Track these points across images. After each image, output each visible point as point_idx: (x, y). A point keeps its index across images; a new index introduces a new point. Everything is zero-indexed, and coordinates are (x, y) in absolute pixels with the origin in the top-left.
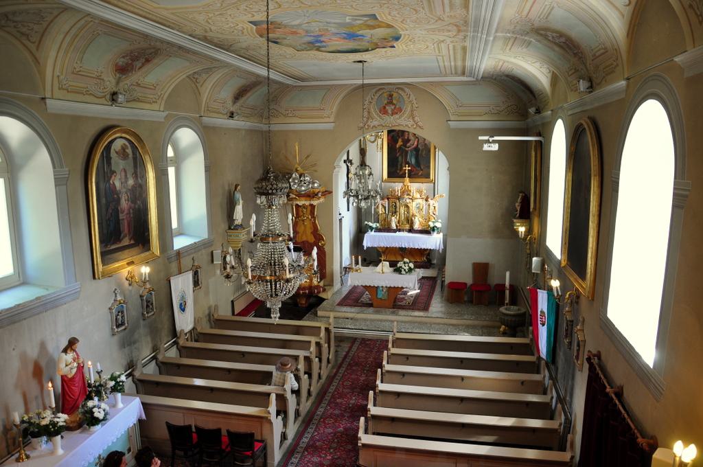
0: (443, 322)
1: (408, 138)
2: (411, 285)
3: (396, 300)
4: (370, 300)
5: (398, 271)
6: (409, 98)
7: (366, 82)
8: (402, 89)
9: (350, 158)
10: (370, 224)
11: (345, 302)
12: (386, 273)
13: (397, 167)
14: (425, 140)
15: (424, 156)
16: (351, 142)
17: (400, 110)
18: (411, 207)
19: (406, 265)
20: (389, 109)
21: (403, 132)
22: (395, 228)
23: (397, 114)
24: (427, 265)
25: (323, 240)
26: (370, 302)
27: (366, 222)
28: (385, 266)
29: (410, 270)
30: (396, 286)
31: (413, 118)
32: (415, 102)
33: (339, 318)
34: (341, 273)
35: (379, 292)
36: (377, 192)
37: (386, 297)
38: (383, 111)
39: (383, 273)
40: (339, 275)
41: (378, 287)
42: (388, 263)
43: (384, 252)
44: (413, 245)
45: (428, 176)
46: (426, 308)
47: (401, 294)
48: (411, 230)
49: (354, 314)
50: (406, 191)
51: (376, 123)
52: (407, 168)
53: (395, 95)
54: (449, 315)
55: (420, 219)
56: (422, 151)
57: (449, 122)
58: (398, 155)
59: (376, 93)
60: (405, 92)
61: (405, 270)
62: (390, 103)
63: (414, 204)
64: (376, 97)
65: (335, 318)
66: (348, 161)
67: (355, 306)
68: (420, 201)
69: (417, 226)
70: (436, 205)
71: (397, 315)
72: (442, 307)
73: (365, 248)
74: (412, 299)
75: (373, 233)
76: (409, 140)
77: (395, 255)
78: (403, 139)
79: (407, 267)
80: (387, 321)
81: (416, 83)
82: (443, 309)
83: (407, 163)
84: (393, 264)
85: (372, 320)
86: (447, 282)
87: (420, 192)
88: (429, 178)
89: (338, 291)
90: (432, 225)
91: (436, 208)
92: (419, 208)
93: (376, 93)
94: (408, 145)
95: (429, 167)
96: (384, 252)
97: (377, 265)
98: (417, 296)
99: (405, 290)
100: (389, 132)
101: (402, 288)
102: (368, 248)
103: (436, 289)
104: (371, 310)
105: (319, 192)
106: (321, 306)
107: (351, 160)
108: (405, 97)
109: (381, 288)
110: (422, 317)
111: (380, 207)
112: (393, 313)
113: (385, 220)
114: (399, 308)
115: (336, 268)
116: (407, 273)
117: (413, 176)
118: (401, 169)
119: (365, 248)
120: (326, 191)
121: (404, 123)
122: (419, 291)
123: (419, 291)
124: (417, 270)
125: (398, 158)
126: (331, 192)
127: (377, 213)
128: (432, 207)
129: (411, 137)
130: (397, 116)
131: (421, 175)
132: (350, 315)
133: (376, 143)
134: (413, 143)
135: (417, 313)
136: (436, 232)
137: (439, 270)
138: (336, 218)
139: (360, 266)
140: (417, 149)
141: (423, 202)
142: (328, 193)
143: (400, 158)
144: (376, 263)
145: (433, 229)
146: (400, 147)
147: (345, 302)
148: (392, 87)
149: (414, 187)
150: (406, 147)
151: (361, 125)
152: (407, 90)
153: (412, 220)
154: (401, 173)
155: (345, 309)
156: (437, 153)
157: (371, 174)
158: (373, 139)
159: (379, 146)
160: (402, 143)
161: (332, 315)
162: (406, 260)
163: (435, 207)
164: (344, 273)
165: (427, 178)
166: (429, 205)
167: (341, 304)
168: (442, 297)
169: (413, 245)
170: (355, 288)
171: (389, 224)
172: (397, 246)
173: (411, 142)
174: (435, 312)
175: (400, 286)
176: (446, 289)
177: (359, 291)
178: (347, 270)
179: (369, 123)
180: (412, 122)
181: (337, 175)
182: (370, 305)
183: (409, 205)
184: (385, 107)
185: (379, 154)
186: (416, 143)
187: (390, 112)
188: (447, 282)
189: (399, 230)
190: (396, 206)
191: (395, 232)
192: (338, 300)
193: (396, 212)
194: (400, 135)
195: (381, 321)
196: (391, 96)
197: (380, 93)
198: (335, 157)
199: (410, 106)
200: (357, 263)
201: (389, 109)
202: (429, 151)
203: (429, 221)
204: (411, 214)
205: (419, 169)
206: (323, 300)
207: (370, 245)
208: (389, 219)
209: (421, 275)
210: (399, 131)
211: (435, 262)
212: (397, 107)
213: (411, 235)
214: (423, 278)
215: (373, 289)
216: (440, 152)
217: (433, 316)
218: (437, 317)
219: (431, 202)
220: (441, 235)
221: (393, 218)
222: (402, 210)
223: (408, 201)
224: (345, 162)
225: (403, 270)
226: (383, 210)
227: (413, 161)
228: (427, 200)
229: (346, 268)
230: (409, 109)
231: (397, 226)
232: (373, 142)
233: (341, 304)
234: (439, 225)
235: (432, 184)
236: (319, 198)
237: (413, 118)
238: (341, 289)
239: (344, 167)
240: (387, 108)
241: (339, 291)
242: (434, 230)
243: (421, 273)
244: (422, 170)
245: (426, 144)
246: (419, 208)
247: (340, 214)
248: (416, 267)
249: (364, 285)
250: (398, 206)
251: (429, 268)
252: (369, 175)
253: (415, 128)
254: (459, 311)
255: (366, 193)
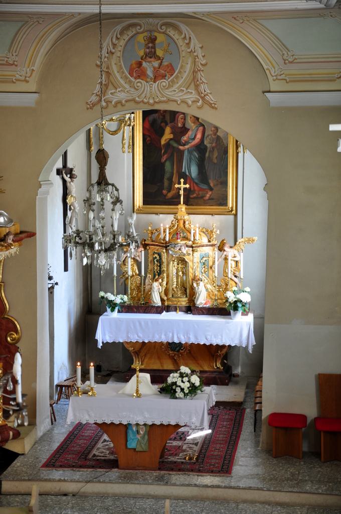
0: (262, 499)
1: (184, 125)
2: (195, 421)
3: (164, 451)
4: (112, 453)
5: (169, 391)
6: (188, 44)
7: (106, 9)
8: (176, 28)
9: (70, 165)
10: (111, 297)
11: (57, 460)
12: (146, 396)
13: (162, 181)
14: (217, 128)
15: (215, 161)
16: (70, 135)
17: (171, 69)
18: (190, 264)
19: (186, 379)
20: (149, 67)
21: (174, 114)
22: (160, 304)
23: (164, 77)
24: (224, 377)
25: (16, 331)
26: (112, 457)
27: (102, 294)
28: (142, 381)
29: (193, 389)
30: (165, 423)
31: (197, 87)
32: (200, 53)
33: (47, 494)
34: (51, 398)
35: (131, 435)
36: (128, 236)
37: (144, 447)
38: (138, 71)
39: (139, 396)
40: (48, 402)
41: (129, 424)
42: (148, 376)
43: (137, 353)
44: (196, 338)
45: (223, 201)
46: (225, 468)
47: (175, 439)
48: (191, 309)
49: (80, 485)
50: (180, 232)
51: (122, 96)
52: (182, 186)
53: (160, 38)
54: (273, 482)
55: (209, 286)
56: (212, 151)
57: (267, 95)
58: (163, 160)
59: (122, 33)
60: (180, 32)
61: (182, 390)
62: (151, 54)
63: (197, 255)
64: (122, 43)
65: (40, 495)
66: (65, 171)
67: (81, 467)
68: (207, 250)
69: (202, 300)
70: (240, 258)
71: (167, 484)
72: (257, 466)
73: (100, 345)
74: (197, 448)
75: (115, 314)
76: (185, 130)
77: (159, 358)
78: (172, 128)
79: (188, 384)
80: (148, 496)
81: (203, 14)
82: (260, 470)
83: (182, 175)
84: (158, 377)
85: (117, 497)
86: (265, 414)
87: (208, 232)
88: (226, 204)
89: (44, 435)
90: (232, 297)
91: (241, 265)
92: (207, 266)
93: (122, 33)
94: (185, 138)
95: (225, 183)
96: (137, 353)
97: (127, 381)
98: (207, 440)
99: (181, 430)
100: (146, 114)
101: (178, 426)
102: (106, 345)
103: (244, 427)
104: (115, 473)
105: (8, 234)
106: (9, 469)
107: (71, 170)
108: (180, 43)
109: (134, 429)
110: (218, 487)
111: (130, 261)
112: (160, 480)
113: (138, 288)
114: (172, 470)
115: (43, 388)
116: (186, 395)
117: (193, 200)
118: (170, 189)
119: (100, 345)
120: (21, 232)
121: (178, 96)
122: (210, 431)
123: (210, 431)
124: (207, 389)
125: (163, 165)
126: (32, 235)
127: (122, 274)
128: (231, 264)
129: (190, 124)
130: (164, 83)
131: (210, 199)
132: (71, 487)
133: (120, 134)
134: (194, 136)
135: (208, 480)
136: (240, 311)
137: (247, 387)
138: (43, 286)
139: (91, 382)
140: (201, 148)
141: (212, 253)
142: (26, 236)
143: (168, 166)
144: (125, 375)
145: (235, 306)
146: (168, 145)
147: (57, 460)
148: (156, 21)
149: (196, 222)
150: (180, 144)
151: (94, 99)
152: (183, 27)
153: (192, 288)
154: (170, 195)
155: (57, 474)
156: (240, 155)
157: (117, 201)
158: (113, 126)
159: (126, 141)
160: (172, 136)
161: (35, 488)
162: (184, 369)
163: (237, 262)
164: (56, 397)
165: (221, 205)
166: (226, 259)
167: (51, 463)
168: (257, 443)
169: (196, 338)
170: (79, 427)
171: (148, 295)
172: (164, 338)
173: (190, 133)
174: (247, 477)
175: (173, 423)
176: (264, 429)
177: (88, 433)
178: (64, 391)
179: (109, 96)
180: (194, 96)
181: (46, 199)
182: (112, 464)
183: (186, 258)
184: (140, 64)
185: (127, 157)
186: (199, 136)
187: (150, 73)
188: (265, 414)
189: (168, 309)
190: (160, 261)
191: (160, 313)
192: (45, 457)
193: (160, 273)
194: (168, 118)
195: (135, 497)
196: (153, 40)
197: (130, 33)
198: (39, 166)
199: (190, 61)
200: (85, 376)
201: (149, 67)
202: (226, 152)
203: (226, 290)
204: (191, 276)
205: (205, 187)
206: (15, 455)
207: (109, 339)
208: (147, 287)
209: (214, 399)
210: (165, 111)
211: (238, 370)
212: (165, 63)
213: (190, 317)
214: (218, 404)
215: (119, 430)
216: (248, 154)
217: (242, 484)
218: (250, 488)
219: (230, 252)
220: (250, 318)
221: (156, 284)
222: (173, 268)
223: (185, 250)
224: (59, 172)
225: (178, 390)
226: (136, 267)
227: (194, 171)
228: (221, 249)
229: (60, 386)
230: (189, 66)
231: (162, 300)
232: (114, 133)
233: (51, 463)
234: (245, 297)
235: (232, 217)
236: (9, 246)
237: (197, 87)
238: (50, 431)
239: (57, 181)
240: (144, 64)
241: (48, 435)
242: (236, 308)
243: (213, 394)
244: (211, 189)
245: (218, 138)
246: (207, 266)
247: (50, 278)
248: (206, 382)
249: (100, 422)
250: (164, 260)
251: (227, 384)
252: (114, 203)
253: (199, 108)
254: (293, 474)
255: (108, 239)
